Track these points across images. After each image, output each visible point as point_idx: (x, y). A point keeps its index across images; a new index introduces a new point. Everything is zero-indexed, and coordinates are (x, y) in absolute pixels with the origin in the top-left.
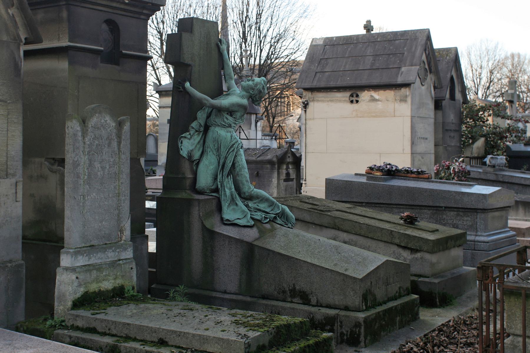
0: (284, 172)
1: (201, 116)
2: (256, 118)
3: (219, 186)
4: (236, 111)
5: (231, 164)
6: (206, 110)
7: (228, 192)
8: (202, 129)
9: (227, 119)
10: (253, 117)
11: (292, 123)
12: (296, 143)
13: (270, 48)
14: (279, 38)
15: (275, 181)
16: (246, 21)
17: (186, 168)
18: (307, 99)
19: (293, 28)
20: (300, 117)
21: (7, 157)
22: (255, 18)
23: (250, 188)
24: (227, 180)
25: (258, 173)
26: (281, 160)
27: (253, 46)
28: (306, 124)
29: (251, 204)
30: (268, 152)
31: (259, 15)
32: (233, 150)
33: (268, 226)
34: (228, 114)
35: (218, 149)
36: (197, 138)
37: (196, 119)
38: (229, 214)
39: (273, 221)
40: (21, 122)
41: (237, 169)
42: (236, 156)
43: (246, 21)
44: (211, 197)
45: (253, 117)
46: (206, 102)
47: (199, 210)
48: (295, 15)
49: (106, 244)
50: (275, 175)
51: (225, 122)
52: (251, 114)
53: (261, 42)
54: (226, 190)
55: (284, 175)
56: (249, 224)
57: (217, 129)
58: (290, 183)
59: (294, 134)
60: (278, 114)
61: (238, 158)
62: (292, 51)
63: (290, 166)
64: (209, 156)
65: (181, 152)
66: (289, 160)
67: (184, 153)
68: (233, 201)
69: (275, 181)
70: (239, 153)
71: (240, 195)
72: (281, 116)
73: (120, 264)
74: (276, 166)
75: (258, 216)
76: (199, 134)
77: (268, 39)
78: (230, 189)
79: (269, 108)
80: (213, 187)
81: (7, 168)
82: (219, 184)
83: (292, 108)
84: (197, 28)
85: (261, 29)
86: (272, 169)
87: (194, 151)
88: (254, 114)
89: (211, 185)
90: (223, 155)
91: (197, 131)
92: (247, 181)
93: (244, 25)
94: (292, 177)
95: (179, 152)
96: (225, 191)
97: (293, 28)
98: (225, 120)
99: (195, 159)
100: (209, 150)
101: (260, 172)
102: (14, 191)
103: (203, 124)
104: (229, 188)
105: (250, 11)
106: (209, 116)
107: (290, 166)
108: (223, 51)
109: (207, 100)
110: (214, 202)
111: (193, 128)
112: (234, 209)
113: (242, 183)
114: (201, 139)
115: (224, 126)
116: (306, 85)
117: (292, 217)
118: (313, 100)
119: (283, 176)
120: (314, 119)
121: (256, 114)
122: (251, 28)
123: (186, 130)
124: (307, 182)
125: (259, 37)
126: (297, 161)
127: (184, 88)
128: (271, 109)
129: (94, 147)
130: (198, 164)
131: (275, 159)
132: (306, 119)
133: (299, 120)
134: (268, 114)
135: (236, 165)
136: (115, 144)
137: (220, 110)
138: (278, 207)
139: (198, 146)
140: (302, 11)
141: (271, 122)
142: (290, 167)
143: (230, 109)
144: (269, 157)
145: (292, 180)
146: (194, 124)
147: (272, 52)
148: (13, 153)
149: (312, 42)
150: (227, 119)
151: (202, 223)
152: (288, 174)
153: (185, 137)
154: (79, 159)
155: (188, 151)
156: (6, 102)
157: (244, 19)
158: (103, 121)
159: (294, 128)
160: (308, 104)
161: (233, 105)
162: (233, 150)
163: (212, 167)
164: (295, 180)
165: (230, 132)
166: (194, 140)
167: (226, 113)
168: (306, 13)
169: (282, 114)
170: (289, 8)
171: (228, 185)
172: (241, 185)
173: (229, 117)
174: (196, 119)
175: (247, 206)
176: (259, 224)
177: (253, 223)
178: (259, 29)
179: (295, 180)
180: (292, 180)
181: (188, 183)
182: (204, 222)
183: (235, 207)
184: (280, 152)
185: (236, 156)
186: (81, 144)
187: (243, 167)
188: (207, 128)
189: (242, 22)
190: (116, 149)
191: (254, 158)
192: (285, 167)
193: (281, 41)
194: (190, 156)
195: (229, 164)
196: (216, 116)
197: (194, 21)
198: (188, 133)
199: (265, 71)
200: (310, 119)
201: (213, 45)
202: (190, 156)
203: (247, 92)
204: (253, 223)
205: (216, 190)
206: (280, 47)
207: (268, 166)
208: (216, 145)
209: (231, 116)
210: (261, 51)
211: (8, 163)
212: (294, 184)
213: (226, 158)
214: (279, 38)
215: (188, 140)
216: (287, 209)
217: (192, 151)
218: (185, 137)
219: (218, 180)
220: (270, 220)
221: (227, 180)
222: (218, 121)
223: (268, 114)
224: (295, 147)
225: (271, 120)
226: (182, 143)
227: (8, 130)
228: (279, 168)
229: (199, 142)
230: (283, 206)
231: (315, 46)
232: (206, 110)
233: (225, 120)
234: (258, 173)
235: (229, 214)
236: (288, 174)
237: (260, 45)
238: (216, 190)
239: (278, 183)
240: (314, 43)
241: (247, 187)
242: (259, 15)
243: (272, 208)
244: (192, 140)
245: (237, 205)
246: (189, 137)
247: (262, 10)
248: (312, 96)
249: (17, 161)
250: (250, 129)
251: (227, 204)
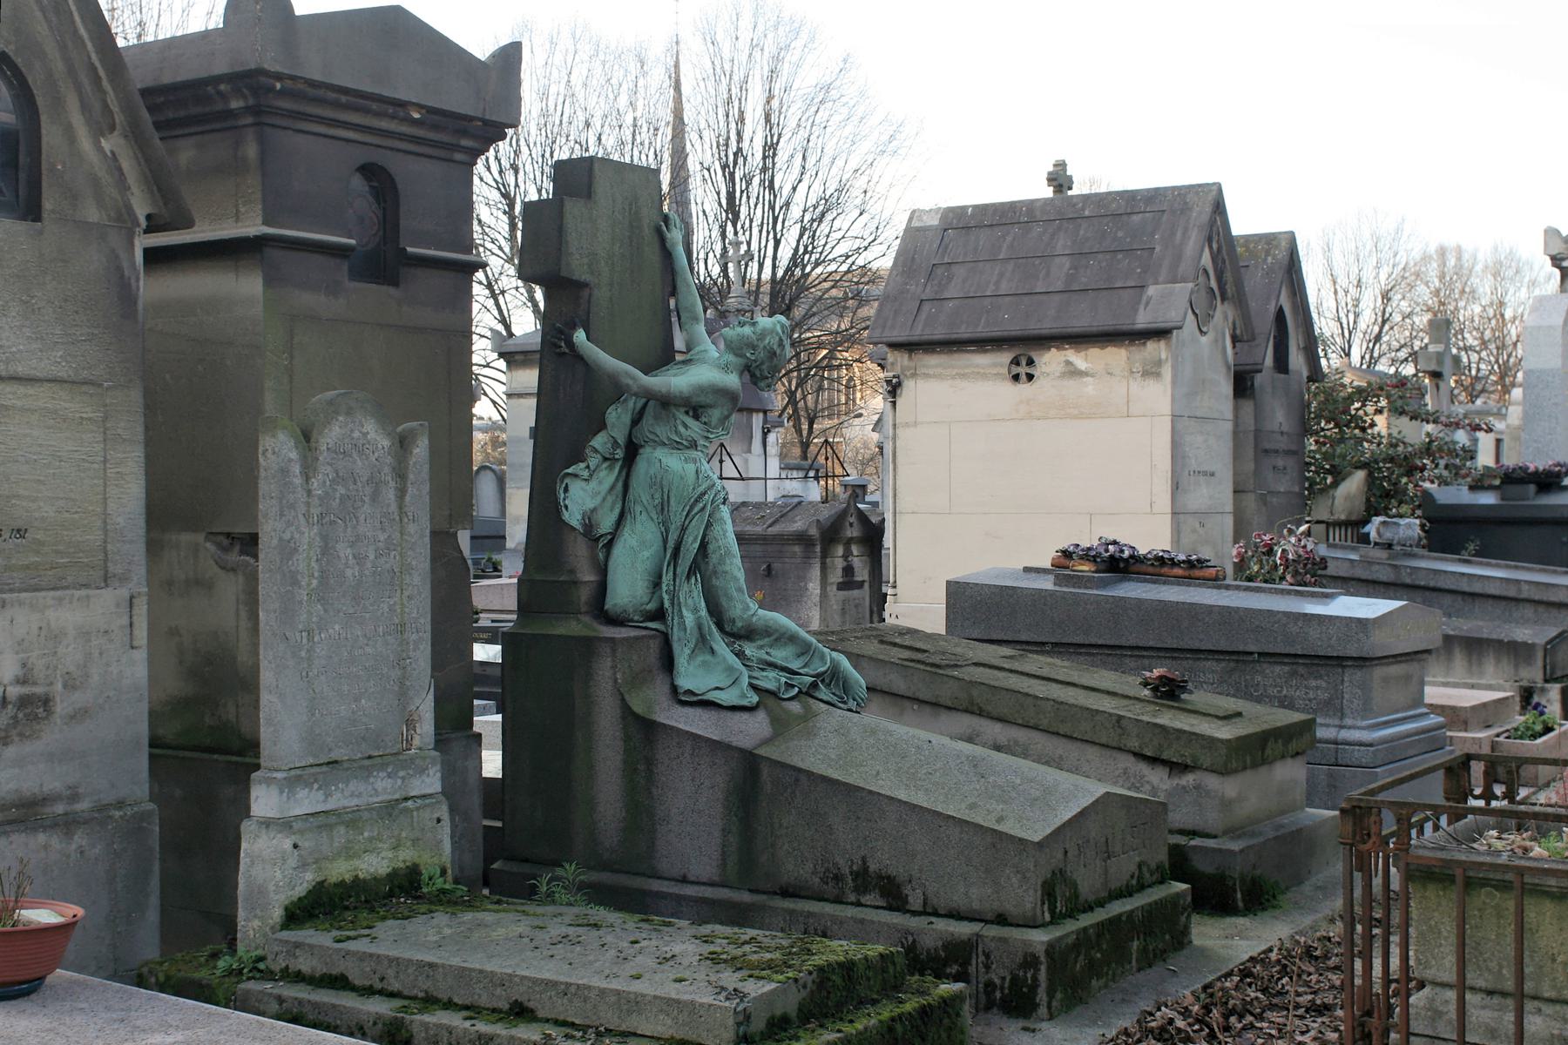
0: (840, 564)
1: (618, 418)
2: (765, 421)
3: (667, 604)
4: (711, 406)
5: (696, 545)
6: (631, 404)
7: (689, 618)
8: (620, 454)
9: (686, 426)
10: (757, 420)
11: (858, 434)
12: (871, 488)
13: (801, 236)
14: (825, 208)
15: (814, 587)
16: (735, 163)
17: (579, 553)
18: (898, 371)
19: (861, 183)
20: (879, 420)
21: (106, 532)
22: (759, 155)
23: (747, 608)
24: (686, 587)
25: (769, 568)
26: (831, 534)
27: (755, 231)
28: (894, 438)
29: (749, 650)
30: (796, 512)
31: (770, 149)
32: (703, 509)
33: (795, 707)
34: (687, 413)
35: (663, 507)
36: (608, 478)
37: (602, 426)
38: (691, 677)
39: (807, 694)
40: (141, 437)
41: (714, 559)
42: (709, 525)
43: (735, 163)
44: (644, 633)
45: (757, 420)
46: (630, 382)
47: (614, 667)
48: (865, 147)
49: (370, 757)
50: (816, 572)
51: (681, 436)
52: (751, 411)
53: (775, 219)
54: (685, 613)
55: (839, 572)
56: (745, 703)
57: (660, 453)
58: (856, 593)
59: (865, 463)
60: (823, 410)
61: (717, 528)
62: (857, 243)
63: (855, 550)
64: (639, 526)
65: (566, 516)
66: (853, 532)
67: (573, 517)
68: (703, 642)
69: (814, 587)
70: (717, 516)
71: (720, 626)
72: (830, 417)
73: (406, 810)
74: (818, 549)
75: (770, 680)
76: (611, 468)
77: (795, 212)
78: (695, 610)
79: (799, 395)
80: (649, 607)
81: (106, 560)
82: (666, 597)
83: (858, 395)
84: (602, 186)
85: (777, 186)
86: (807, 557)
87: (600, 512)
88: (758, 411)
89: (646, 599)
90: (677, 520)
91: (606, 459)
92: (740, 590)
93: (732, 175)
94: (859, 579)
95: (558, 512)
96: (682, 617)
97: (861, 183)
98: (682, 430)
99: (602, 531)
100: (638, 508)
101: (776, 566)
102: (125, 621)
103: (621, 441)
104: (691, 610)
105: (746, 137)
106: (636, 421)
107: (855, 550)
108: (674, 245)
109: (634, 378)
110: (655, 646)
111: (596, 451)
112: (704, 663)
113: (726, 595)
114: (617, 480)
115: (677, 446)
116: (895, 333)
117: (857, 682)
118: (914, 375)
119: (836, 576)
120: (916, 424)
121: (765, 412)
122: (749, 184)
123: (578, 457)
124: (898, 591)
125: (772, 208)
126: (873, 537)
127: (571, 344)
128: (804, 397)
129: (335, 504)
130: (609, 545)
131: (814, 532)
132: (895, 425)
133: (878, 426)
134: (795, 410)
135: (711, 547)
136: (390, 495)
137: (666, 403)
138: (822, 657)
139: (610, 499)
140: (885, 138)
141: (805, 433)
142: (855, 553)
143: (695, 400)
144: (798, 525)
145: (860, 585)
146: (599, 441)
147: (806, 247)
148: (120, 520)
149: (910, 219)
150: (686, 426)
151: (623, 700)
152: (848, 570)
153: (576, 476)
154: (297, 536)
155: (584, 515)
156: (100, 385)
157: (731, 158)
158: (356, 434)
159: (866, 446)
160: (899, 384)
161: (701, 389)
162: (703, 509)
163: (646, 554)
164: (866, 585)
165: (695, 461)
166: (600, 483)
167: (683, 410)
168: (895, 143)
169: (832, 410)
170: (849, 129)
171: (690, 601)
172: (724, 602)
173: (690, 421)
174: (602, 426)
175: (740, 654)
176: (771, 701)
177: (755, 699)
178: (771, 186)
179: (866, 585)
180: (860, 585)
181: (584, 595)
182: (627, 697)
183: (708, 657)
184: (826, 513)
185: (709, 525)
186: (301, 495)
187: (728, 553)
188: (632, 451)
189: (724, 167)
190: (394, 507)
191: (759, 529)
192: (840, 551)
193: (829, 217)
194: (589, 526)
195: (691, 546)
196: (656, 418)
197: (596, 166)
198: (582, 465)
199: (787, 297)
200: (907, 425)
201: (647, 232)
202: (589, 526)
203: (736, 355)
204: (755, 699)
205: (659, 614)
206: (826, 231)
207: (797, 549)
208: (657, 496)
209: (696, 417)
210: (777, 243)
211: (109, 547)
212: (864, 594)
213: (684, 529)
214: (825, 208)
215: (583, 484)
216: (845, 663)
217: (594, 510)
218: (576, 476)
219: (664, 588)
220: (800, 692)
221: (686, 587)
222: (663, 431)
223: (795, 410)
224: (868, 499)
225: (805, 427)
226: (566, 490)
227: (105, 461)
228: (825, 555)
229: (613, 487)
230: (834, 654)
231: (918, 229)
232: (631, 404)
233: (682, 430)
234: (769, 568)
235: (691, 677)
236: (848, 570)
237: (774, 228)
238: (659, 614)
239: (824, 595)
240: (915, 224)
241: (739, 606)
242: (770, 149)
243: (806, 658)
244: (593, 484)
245: (713, 652)
246: (586, 474)
247: (780, 135)
248: (912, 364)
249: (131, 542)
250: (749, 451)
251: (687, 651)
